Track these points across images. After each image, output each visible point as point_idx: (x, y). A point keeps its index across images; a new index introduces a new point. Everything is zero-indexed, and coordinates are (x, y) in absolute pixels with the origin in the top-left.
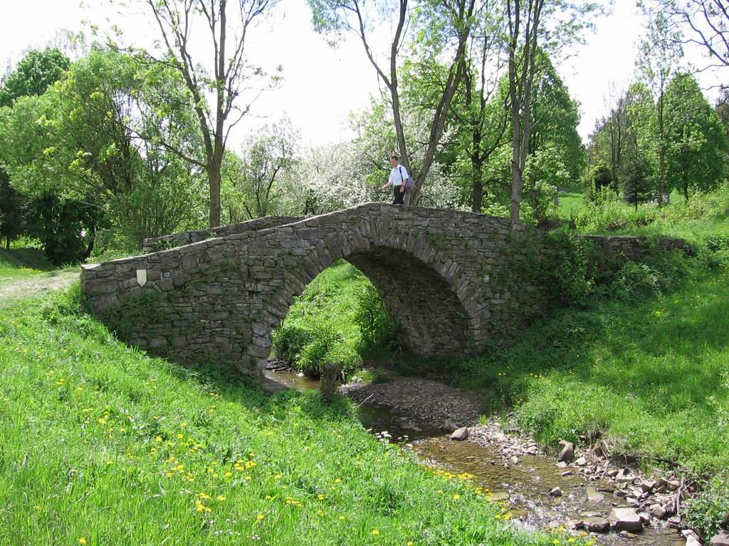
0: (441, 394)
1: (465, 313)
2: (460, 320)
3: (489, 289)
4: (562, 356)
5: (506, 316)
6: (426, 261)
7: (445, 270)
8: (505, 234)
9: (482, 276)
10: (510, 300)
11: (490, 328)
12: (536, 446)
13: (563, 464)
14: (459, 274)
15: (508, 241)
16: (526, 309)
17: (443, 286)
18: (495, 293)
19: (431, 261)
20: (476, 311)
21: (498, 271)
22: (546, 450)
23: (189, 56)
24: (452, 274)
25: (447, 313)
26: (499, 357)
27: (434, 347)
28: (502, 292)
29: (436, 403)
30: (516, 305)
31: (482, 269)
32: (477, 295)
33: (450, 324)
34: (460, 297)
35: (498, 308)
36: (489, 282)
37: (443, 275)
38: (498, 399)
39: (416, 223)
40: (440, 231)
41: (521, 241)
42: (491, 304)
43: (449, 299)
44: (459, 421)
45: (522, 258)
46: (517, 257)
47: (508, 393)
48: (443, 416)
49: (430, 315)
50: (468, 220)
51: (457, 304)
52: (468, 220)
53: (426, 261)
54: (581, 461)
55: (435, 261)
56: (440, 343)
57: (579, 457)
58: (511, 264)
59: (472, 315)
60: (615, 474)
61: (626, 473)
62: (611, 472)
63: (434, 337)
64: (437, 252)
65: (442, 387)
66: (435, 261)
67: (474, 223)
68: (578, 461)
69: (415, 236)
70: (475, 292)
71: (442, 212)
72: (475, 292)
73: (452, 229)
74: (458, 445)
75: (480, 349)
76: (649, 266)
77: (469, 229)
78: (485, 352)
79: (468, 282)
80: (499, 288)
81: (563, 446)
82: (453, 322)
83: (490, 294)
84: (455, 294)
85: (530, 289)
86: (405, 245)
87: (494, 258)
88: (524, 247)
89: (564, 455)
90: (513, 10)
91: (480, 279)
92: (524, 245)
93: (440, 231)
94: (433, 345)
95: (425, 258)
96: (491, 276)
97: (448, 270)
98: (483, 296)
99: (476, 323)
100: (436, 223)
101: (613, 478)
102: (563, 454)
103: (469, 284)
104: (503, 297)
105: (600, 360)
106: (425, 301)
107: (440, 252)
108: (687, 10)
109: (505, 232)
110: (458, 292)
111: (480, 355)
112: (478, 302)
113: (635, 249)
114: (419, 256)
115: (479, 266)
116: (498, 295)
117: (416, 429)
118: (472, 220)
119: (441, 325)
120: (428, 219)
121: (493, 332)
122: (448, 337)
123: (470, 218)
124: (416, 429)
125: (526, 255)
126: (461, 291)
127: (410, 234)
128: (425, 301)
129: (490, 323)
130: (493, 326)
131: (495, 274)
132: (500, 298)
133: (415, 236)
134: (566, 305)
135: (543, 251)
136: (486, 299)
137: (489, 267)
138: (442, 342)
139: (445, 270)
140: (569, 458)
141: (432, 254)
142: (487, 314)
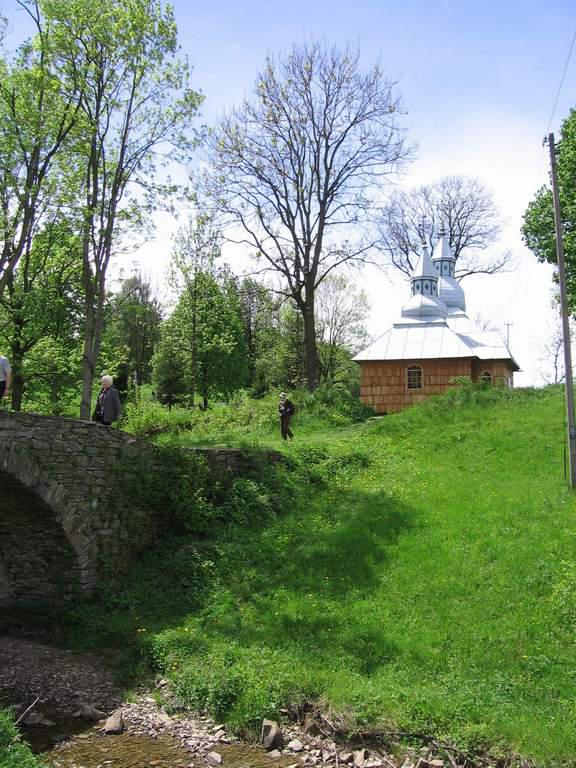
0: (50, 661)
1: (71, 549)
2: (59, 555)
3: (97, 518)
4: (179, 599)
5: (115, 550)
6: (29, 484)
7: (49, 495)
8: (116, 448)
9: (90, 501)
10: (119, 529)
11: (99, 565)
12: (223, 729)
13: (275, 753)
14: (66, 500)
15: (119, 456)
16: (136, 540)
17: (43, 516)
18: (103, 521)
19: (35, 484)
20: (82, 544)
21: (107, 493)
22: (241, 735)
23: (284, 222)
24: (57, 500)
25: (40, 549)
26: (116, 605)
27: (15, 592)
28: (111, 520)
29: (51, 676)
30: (125, 535)
31: (90, 493)
32: (84, 525)
33: (44, 563)
34: (65, 528)
35: (107, 540)
36: (98, 508)
37: (48, 501)
38: (134, 668)
39: (20, 434)
40: (47, 445)
41: (132, 456)
42: (99, 536)
43: (48, 532)
44: (95, 701)
45: (134, 477)
46: (128, 476)
47: (152, 655)
48: (68, 696)
49: (13, 552)
50: (76, 430)
51: (61, 538)
52: (76, 430)
53: (29, 484)
54: (295, 744)
55: (38, 484)
56: (25, 587)
57: (290, 740)
58: (122, 484)
59: (80, 551)
60: (351, 759)
61: (366, 756)
62: (345, 757)
63: (15, 578)
64: (41, 472)
65: (46, 651)
66: (38, 484)
67: (83, 434)
68: (291, 745)
69: (17, 452)
70: (82, 521)
71: (48, 420)
72: (82, 521)
73: (59, 442)
74: (112, 740)
75: (88, 594)
76: (258, 482)
77: (77, 441)
78: (96, 597)
79: (74, 510)
80: (108, 515)
81: (268, 728)
82: (49, 560)
83: (98, 524)
84: (59, 526)
85: (141, 514)
86: (5, 464)
87: (103, 478)
88: (135, 464)
89: (274, 740)
90: (92, 183)
91: (88, 505)
92: (135, 460)
93: (47, 445)
94: (13, 589)
95: (27, 480)
96: (100, 500)
97: (53, 495)
98: (91, 526)
99: (83, 561)
100: (42, 434)
101: (350, 764)
102: (271, 740)
103: (76, 513)
104: (113, 526)
105: (220, 601)
106: (8, 533)
107: (45, 472)
108: (240, 209)
109: (116, 445)
110: (63, 523)
111: (90, 602)
112: (86, 535)
113: (239, 464)
114: (21, 478)
115: (88, 488)
116: (106, 525)
117: (48, 723)
118: (81, 430)
119: (28, 565)
120: (33, 429)
121: (102, 571)
122: (38, 579)
123: (79, 428)
124: (48, 723)
125: (137, 473)
126: (68, 521)
127: (13, 448)
128: (8, 533)
129: (99, 560)
130: (103, 563)
131: (103, 497)
132: (109, 527)
133: (17, 452)
134: (181, 531)
135: (155, 468)
136: (94, 530)
137: (99, 489)
138: (27, 585)
139: (49, 495)
140: (279, 743)
141: (36, 474)
142: (96, 549)
